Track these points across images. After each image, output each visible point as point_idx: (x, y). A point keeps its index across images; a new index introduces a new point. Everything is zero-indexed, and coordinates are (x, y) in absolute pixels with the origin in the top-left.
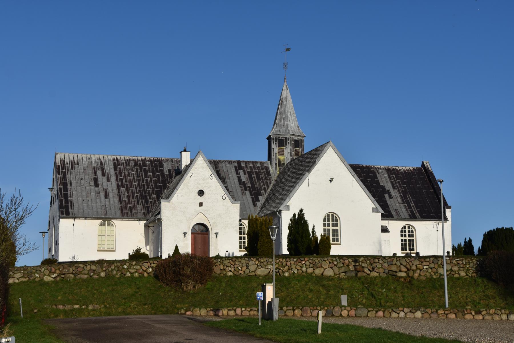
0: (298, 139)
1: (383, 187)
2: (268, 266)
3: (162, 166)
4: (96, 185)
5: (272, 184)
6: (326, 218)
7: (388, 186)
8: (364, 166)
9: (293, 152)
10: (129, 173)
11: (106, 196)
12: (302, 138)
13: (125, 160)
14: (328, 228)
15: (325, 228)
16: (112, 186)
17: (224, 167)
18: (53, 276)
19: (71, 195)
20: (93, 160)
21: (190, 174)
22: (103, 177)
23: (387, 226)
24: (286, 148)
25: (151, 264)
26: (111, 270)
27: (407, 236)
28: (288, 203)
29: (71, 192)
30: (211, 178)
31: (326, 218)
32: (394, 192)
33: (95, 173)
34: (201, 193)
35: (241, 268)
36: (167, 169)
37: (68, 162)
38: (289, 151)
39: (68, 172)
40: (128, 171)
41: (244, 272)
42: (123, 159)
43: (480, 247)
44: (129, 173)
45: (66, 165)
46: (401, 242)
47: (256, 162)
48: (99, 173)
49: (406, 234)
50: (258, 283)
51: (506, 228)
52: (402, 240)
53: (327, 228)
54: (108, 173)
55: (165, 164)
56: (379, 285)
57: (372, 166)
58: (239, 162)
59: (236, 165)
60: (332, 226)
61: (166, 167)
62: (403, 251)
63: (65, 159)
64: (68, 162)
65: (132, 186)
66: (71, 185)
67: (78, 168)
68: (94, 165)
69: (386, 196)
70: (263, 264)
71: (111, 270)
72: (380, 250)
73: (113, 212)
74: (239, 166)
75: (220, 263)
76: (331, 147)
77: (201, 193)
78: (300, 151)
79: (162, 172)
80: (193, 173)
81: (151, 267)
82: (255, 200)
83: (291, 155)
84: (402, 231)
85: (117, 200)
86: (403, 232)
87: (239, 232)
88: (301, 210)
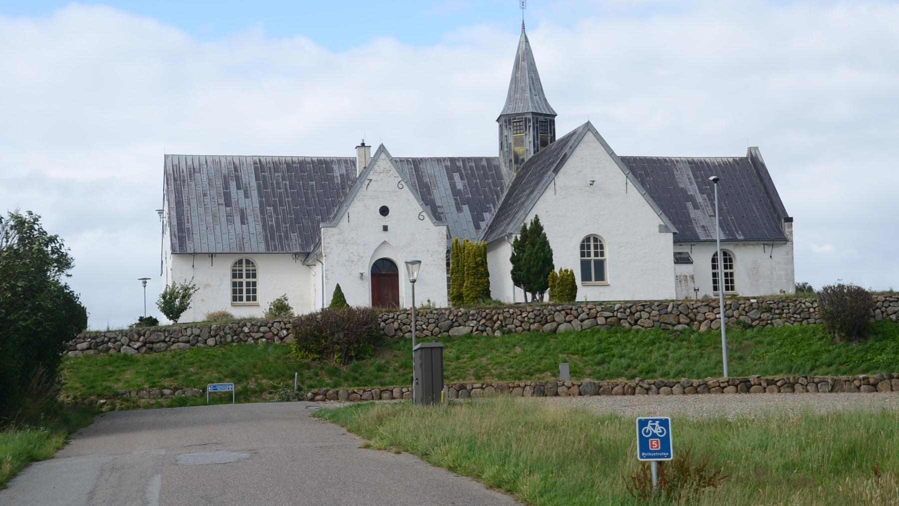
1: (684, 191)
2: (469, 322)
3: (332, 170)
4: (228, 204)
7: (693, 189)
9: (538, 140)
10: (278, 183)
11: (243, 221)
12: (549, 118)
13: (273, 163)
18: (136, 346)
19: (188, 220)
20: (223, 165)
21: (367, 182)
22: (239, 191)
23: (690, 253)
25: (285, 324)
26: (223, 334)
27: (245, 298)
29: (189, 216)
30: (400, 186)
31: (585, 243)
32: (700, 199)
33: (226, 186)
34: (384, 211)
35: (427, 326)
36: (338, 175)
37: (185, 170)
38: (532, 139)
39: (184, 185)
40: (278, 179)
41: (432, 331)
42: (269, 162)
44: (278, 183)
45: (181, 174)
46: (713, 277)
47: (481, 159)
48: (233, 185)
51: (561, 271)
54: (246, 184)
55: (335, 167)
58: (453, 160)
59: (449, 164)
61: (337, 171)
63: (179, 164)
64: (185, 170)
66: (189, 204)
67: (202, 178)
68: (225, 171)
69: (689, 205)
71: (223, 334)
73: (254, 244)
74: (453, 165)
75: (393, 320)
77: (384, 211)
81: (285, 328)
82: (477, 220)
83: (534, 146)
85: (259, 228)
87: (580, 262)
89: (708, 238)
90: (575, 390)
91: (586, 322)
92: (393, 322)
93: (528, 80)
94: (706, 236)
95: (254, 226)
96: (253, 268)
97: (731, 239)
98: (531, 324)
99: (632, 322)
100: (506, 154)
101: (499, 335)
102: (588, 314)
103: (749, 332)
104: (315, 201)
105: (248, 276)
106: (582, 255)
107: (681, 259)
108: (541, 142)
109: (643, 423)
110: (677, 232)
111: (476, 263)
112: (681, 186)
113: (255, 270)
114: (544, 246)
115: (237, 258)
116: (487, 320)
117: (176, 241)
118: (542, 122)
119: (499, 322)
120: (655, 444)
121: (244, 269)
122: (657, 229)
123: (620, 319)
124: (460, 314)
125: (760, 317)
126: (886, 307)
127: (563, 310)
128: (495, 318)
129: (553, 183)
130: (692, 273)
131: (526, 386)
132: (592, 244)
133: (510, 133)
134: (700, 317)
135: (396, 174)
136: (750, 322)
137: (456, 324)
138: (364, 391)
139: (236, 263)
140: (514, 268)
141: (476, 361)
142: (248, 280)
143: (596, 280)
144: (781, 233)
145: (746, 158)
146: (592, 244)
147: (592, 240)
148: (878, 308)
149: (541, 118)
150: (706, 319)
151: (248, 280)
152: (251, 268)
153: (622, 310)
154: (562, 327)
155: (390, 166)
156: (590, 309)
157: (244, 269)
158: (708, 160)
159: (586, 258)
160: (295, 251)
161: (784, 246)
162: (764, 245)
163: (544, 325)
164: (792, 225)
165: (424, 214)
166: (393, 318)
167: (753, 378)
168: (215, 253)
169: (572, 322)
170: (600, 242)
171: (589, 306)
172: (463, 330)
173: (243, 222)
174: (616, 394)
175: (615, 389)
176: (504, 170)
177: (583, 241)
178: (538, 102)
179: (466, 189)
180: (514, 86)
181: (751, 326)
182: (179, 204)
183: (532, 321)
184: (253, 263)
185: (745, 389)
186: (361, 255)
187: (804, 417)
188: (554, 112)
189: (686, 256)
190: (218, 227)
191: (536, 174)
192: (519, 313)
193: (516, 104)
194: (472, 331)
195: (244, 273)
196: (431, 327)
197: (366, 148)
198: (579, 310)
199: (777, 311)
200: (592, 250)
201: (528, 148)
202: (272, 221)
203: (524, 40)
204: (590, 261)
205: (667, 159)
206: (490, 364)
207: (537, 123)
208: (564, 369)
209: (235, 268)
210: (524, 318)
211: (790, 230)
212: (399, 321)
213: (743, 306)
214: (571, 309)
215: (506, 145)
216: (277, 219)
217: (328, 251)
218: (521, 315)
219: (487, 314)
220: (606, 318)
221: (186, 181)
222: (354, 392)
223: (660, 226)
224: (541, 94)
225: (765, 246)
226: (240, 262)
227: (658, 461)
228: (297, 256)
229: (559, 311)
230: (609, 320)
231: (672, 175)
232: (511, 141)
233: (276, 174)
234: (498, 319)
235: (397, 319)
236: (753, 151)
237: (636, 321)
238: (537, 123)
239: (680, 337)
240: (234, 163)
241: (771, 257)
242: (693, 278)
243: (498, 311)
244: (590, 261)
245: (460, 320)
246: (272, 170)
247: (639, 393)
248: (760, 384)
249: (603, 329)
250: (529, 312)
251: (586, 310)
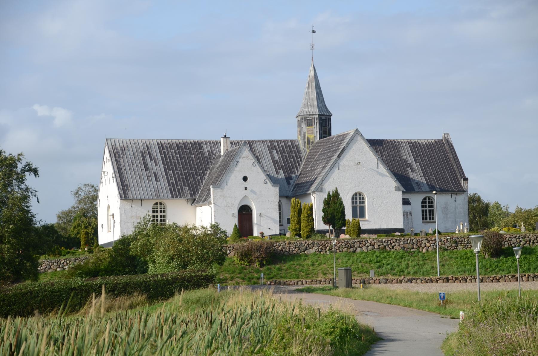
0: (326, 118)
2: (314, 247)
4: (147, 169)
5: (303, 163)
7: (411, 160)
9: (321, 130)
14: (426, 209)
15: (423, 209)
16: (160, 169)
17: (258, 147)
19: (126, 179)
22: (152, 161)
23: (409, 198)
25: (229, 248)
32: (415, 166)
34: (245, 179)
35: (295, 249)
38: (318, 130)
42: (166, 143)
43: (326, 198)
49: (426, 205)
52: (423, 211)
55: (205, 146)
58: (271, 142)
59: (269, 144)
60: (429, 208)
62: (423, 221)
65: (223, 171)
66: (125, 169)
67: (130, 153)
69: (409, 169)
72: (380, 227)
74: (272, 145)
77: (245, 179)
79: (203, 154)
84: (422, 203)
86: (423, 203)
87: (351, 207)
88: (336, 188)
89: (420, 190)
90: (377, 281)
91: (370, 247)
92: (279, 247)
93: (315, 94)
94: (419, 189)
95: (163, 183)
96: (164, 207)
98: (343, 248)
99: (391, 248)
100: (303, 139)
101: (329, 253)
102: (370, 244)
103: (445, 253)
104: (195, 167)
105: (161, 212)
106: (353, 203)
107: (406, 202)
108: (323, 131)
109: (440, 294)
110: (405, 190)
111: (308, 215)
112: (405, 157)
113: (165, 208)
114: (341, 205)
115: (155, 202)
116: (323, 246)
117: (122, 192)
118: (324, 119)
119: (328, 247)
120: (442, 297)
121: (159, 207)
122: (394, 189)
123: (385, 246)
124: (310, 243)
125: (451, 245)
126: (510, 241)
127: (359, 242)
128: (327, 245)
129: (337, 163)
130: (410, 211)
131: (357, 279)
132: (358, 197)
133: (305, 126)
134: (423, 245)
135: (252, 158)
136: (446, 248)
137: (308, 248)
138: (291, 281)
139: (154, 205)
140: (325, 215)
141: (322, 266)
142: (157, 214)
143: (360, 217)
145: (442, 140)
147: (358, 195)
148: (506, 241)
149: (323, 117)
150: (426, 246)
151: (157, 214)
152: (162, 207)
153: (386, 242)
154: (359, 250)
155: (248, 154)
156: (371, 241)
157: (159, 207)
158: (419, 141)
159: (355, 205)
160: (188, 198)
161: (463, 194)
162: (451, 194)
163: (350, 249)
164: (467, 182)
165: (267, 181)
166: (279, 245)
167: (450, 277)
168: (143, 199)
169: (363, 248)
170: (363, 196)
171: (371, 240)
172: (312, 251)
173: (157, 181)
174: (394, 283)
175: (394, 281)
176: (302, 147)
177: (353, 196)
178: (321, 108)
179: (281, 160)
180: (307, 97)
181: (447, 250)
182: (119, 169)
183: (344, 247)
184: (163, 205)
185: (446, 281)
186: (233, 203)
187: (338, 331)
188: (330, 113)
189: (407, 201)
190: (143, 183)
191: (324, 155)
192: (338, 243)
193: (309, 108)
194: (316, 251)
195: (159, 210)
196: (296, 249)
197: (227, 138)
198: (366, 242)
199: (460, 243)
200: (358, 201)
201: (316, 135)
202: (173, 180)
203: (313, 69)
204: (357, 207)
205: (396, 140)
206: (328, 268)
207: (321, 120)
208: (372, 272)
209: (154, 207)
210: (340, 245)
211: (466, 185)
212: (282, 247)
213: (443, 240)
214: (362, 241)
215: (302, 133)
216: (175, 179)
217: (215, 201)
218: (339, 244)
219: (323, 243)
220: (379, 246)
221: (121, 155)
222: (287, 281)
224: (323, 102)
225: (452, 195)
226: (157, 204)
228: (188, 200)
229: (357, 242)
230: (380, 246)
231: (399, 151)
232: (306, 130)
233: (172, 151)
234: (328, 246)
235: (281, 245)
236: (446, 136)
237: (393, 247)
238: (321, 120)
239: (412, 254)
240: (146, 144)
241: (455, 201)
242: (411, 213)
243: (328, 242)
244: (357, 207)
245: (310, 246)
246: (169, 148)
247: (404, 283)
248: (453, 279)
249: (377, 251)
250: (342, 243)
251: (369, 242)
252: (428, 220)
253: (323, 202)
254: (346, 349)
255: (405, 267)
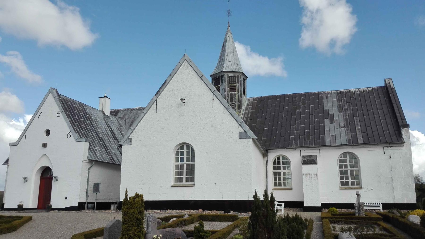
6: (180, 151)
8: (313, 93)
14: (279, 171)
15: (275, 171)
24: (221, 85)
28: (130, 135)
30: (58, 115)
31: (180, 151)
50: (226, 235)
52: (341, 172)
53: (277, 171)
56: (256, 232)
57: (322, 92)
70: (322, 220)
72: (394, 199)
76: (186, 61)
77: (48, 132)
78: (237, 86)
80: (42, 112)
86: (342, 163)
97: (353, 143)
122: (237, 136)
132: (185, 150)
144: (400, 135)
146: (185, 150)
162: (384, 147)
223: (240, 133)
227: (286, 186)
252: (185, 182)
253: (422, 134)
254: (145, 222)
255: (297, 217)
